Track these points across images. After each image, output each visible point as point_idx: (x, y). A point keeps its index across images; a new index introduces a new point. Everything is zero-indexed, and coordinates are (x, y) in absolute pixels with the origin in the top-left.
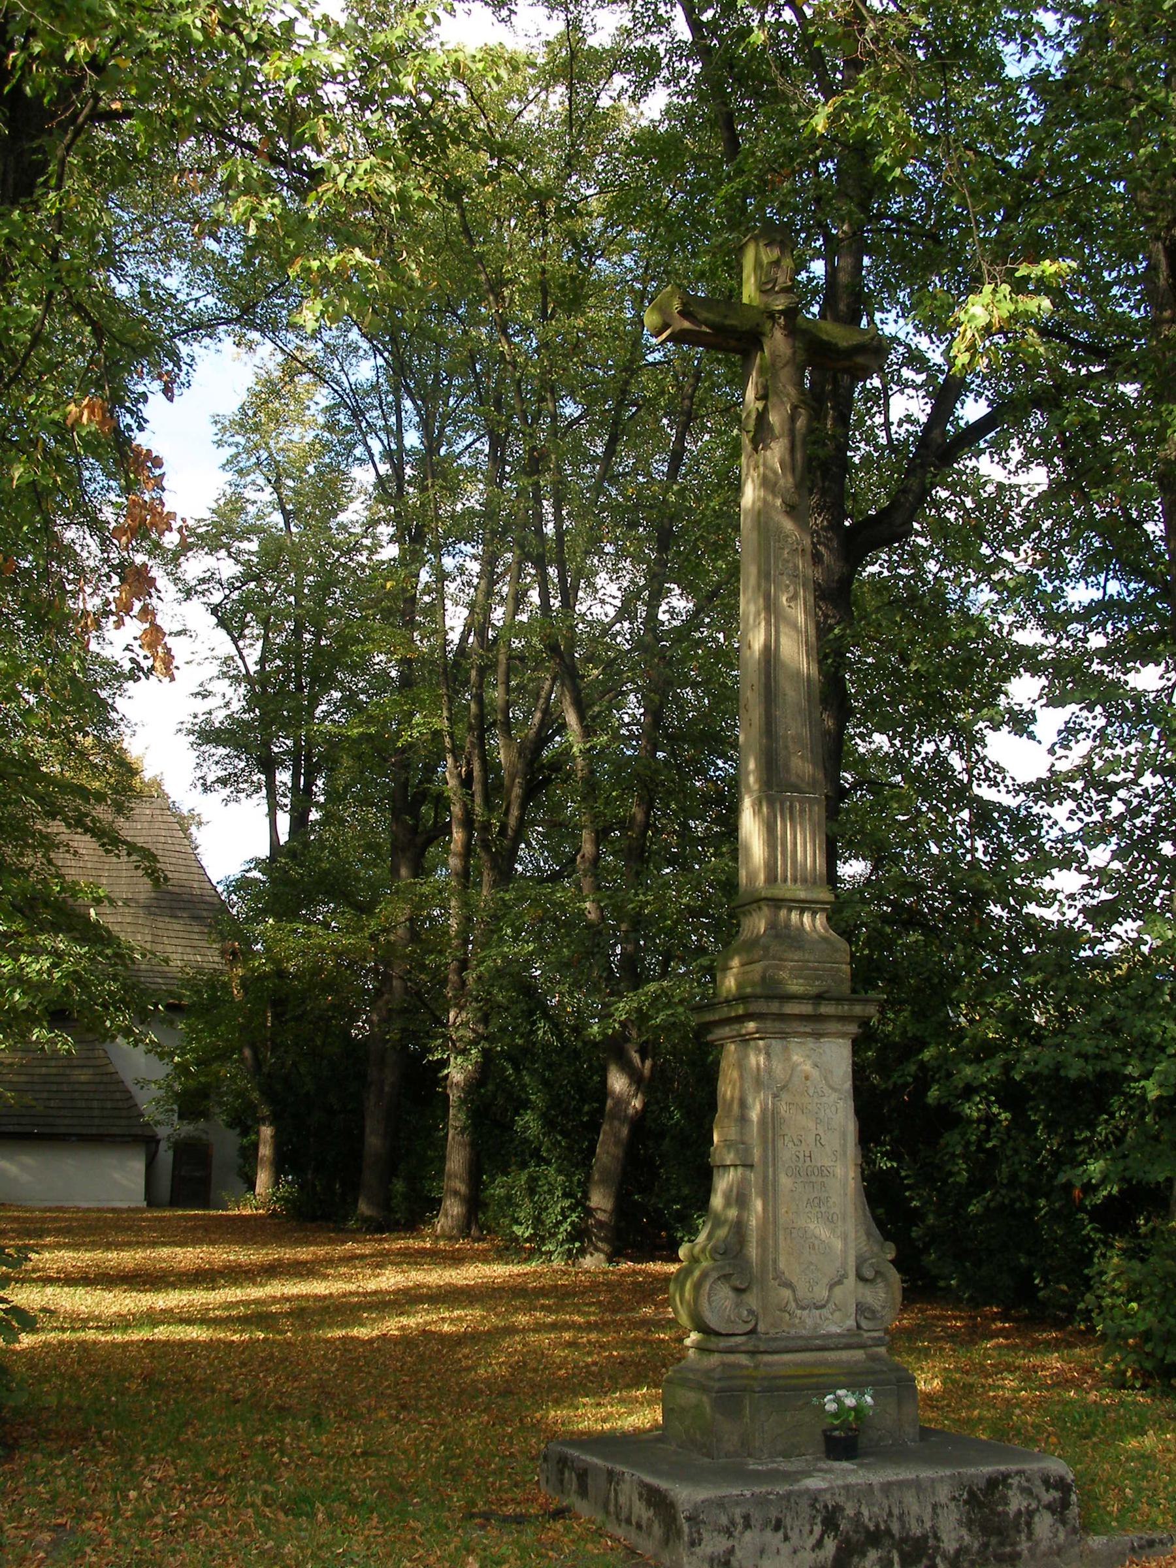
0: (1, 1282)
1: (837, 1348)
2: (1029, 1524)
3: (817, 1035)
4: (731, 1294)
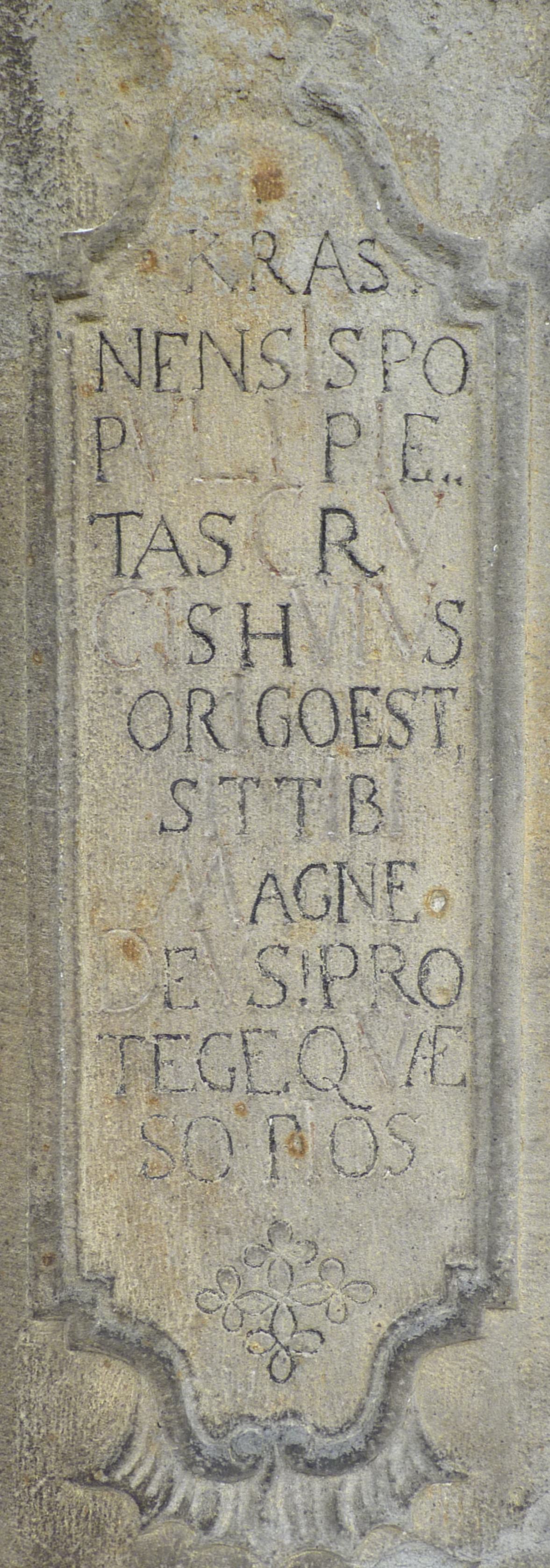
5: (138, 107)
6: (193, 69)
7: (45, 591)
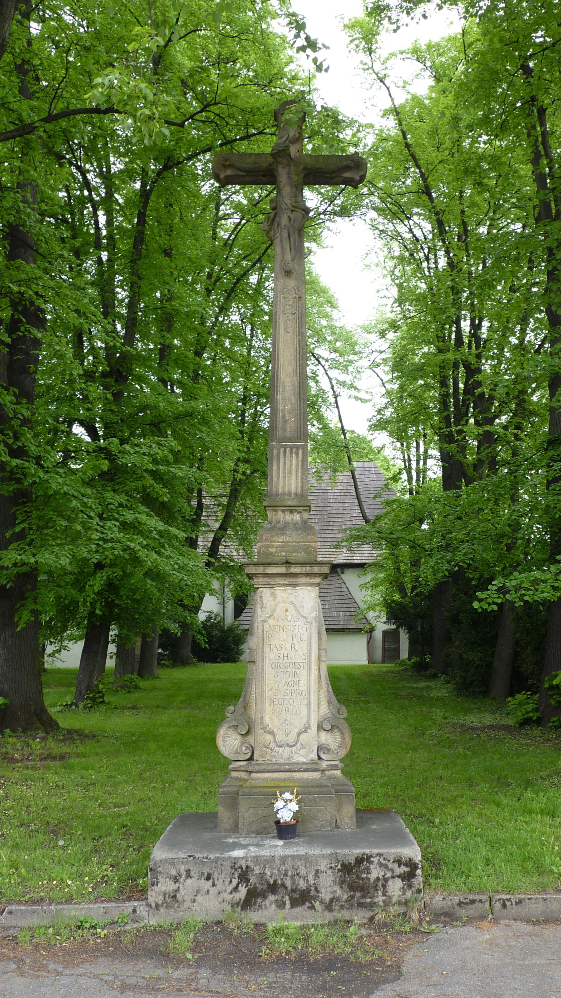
0: (3, 545)
1: (299, 771)
2: (384, 886)
3: (294, 585)
5: (273, 603)
6: (279, 599)
7: (263, 652)
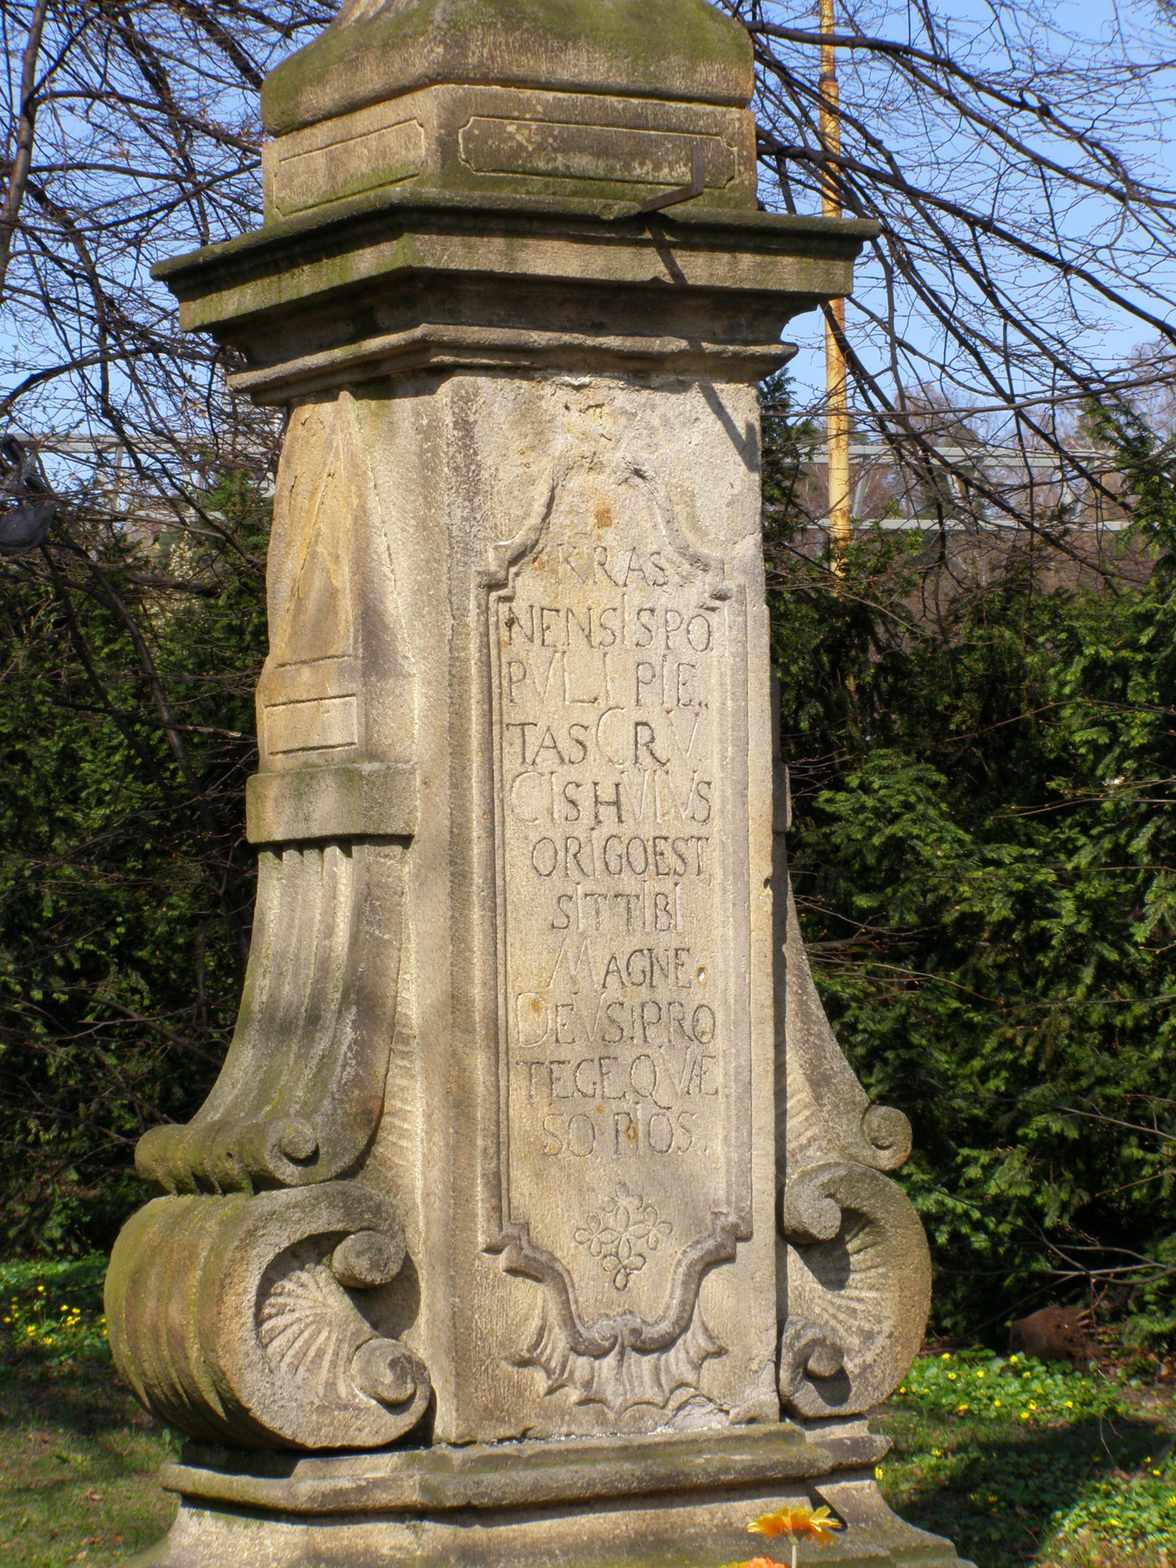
4: (339, 1304)
